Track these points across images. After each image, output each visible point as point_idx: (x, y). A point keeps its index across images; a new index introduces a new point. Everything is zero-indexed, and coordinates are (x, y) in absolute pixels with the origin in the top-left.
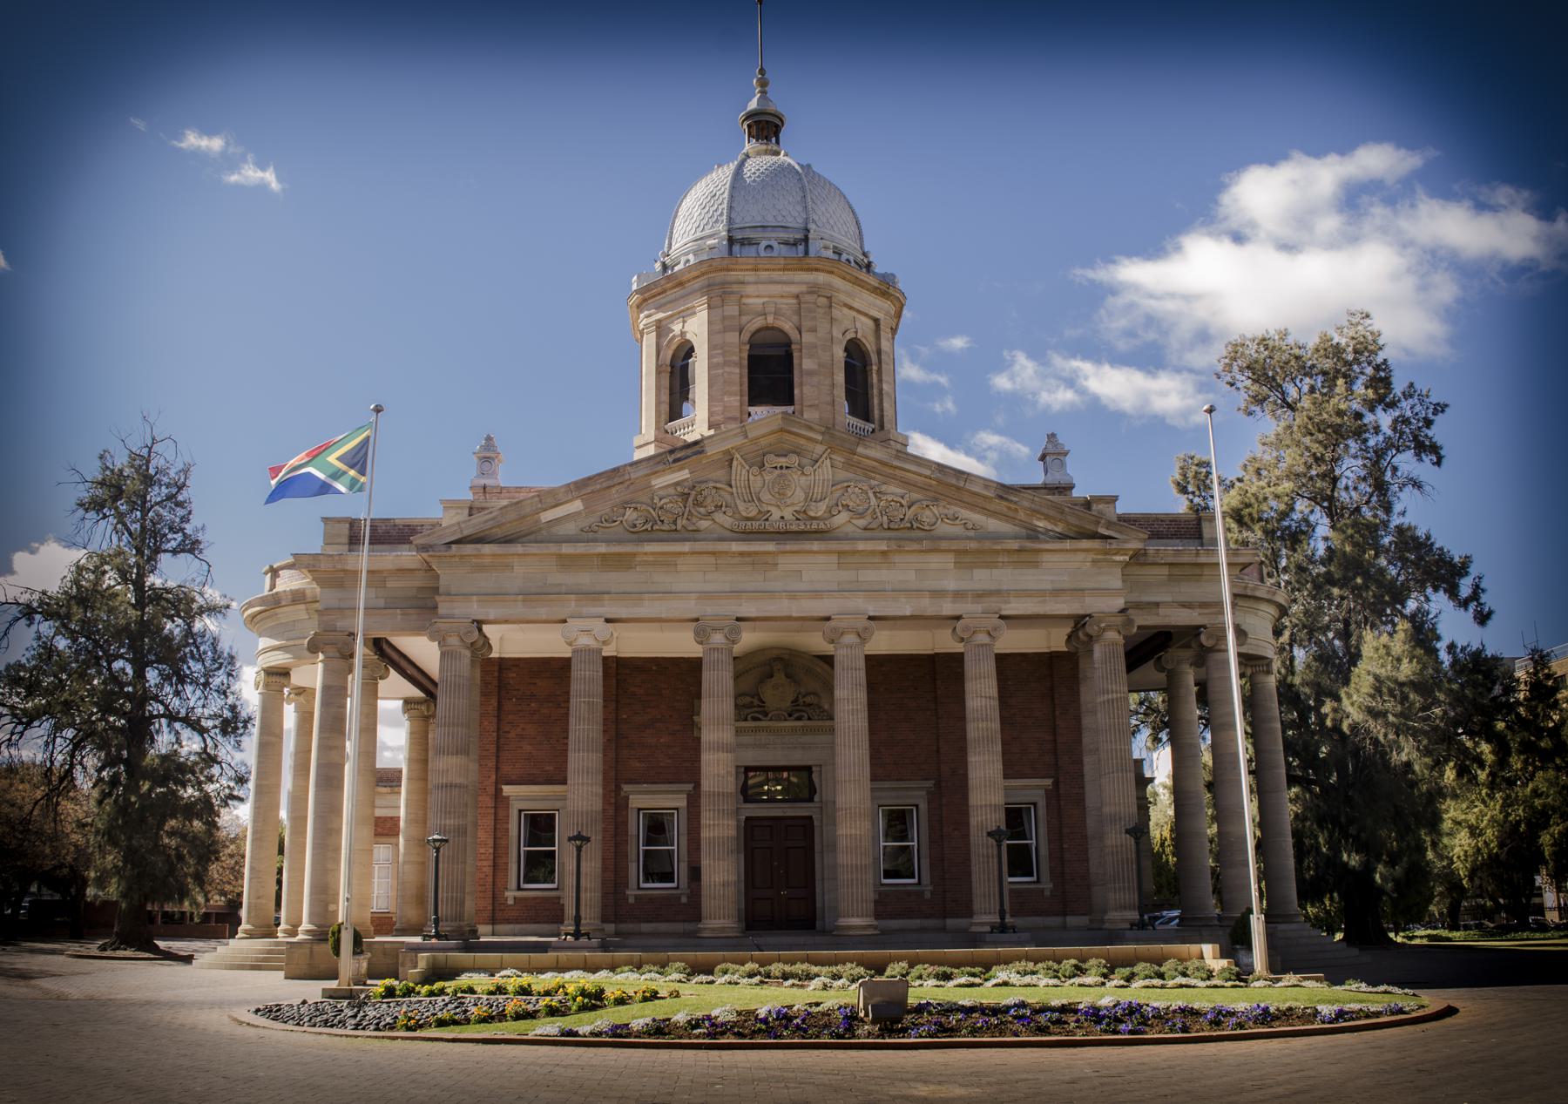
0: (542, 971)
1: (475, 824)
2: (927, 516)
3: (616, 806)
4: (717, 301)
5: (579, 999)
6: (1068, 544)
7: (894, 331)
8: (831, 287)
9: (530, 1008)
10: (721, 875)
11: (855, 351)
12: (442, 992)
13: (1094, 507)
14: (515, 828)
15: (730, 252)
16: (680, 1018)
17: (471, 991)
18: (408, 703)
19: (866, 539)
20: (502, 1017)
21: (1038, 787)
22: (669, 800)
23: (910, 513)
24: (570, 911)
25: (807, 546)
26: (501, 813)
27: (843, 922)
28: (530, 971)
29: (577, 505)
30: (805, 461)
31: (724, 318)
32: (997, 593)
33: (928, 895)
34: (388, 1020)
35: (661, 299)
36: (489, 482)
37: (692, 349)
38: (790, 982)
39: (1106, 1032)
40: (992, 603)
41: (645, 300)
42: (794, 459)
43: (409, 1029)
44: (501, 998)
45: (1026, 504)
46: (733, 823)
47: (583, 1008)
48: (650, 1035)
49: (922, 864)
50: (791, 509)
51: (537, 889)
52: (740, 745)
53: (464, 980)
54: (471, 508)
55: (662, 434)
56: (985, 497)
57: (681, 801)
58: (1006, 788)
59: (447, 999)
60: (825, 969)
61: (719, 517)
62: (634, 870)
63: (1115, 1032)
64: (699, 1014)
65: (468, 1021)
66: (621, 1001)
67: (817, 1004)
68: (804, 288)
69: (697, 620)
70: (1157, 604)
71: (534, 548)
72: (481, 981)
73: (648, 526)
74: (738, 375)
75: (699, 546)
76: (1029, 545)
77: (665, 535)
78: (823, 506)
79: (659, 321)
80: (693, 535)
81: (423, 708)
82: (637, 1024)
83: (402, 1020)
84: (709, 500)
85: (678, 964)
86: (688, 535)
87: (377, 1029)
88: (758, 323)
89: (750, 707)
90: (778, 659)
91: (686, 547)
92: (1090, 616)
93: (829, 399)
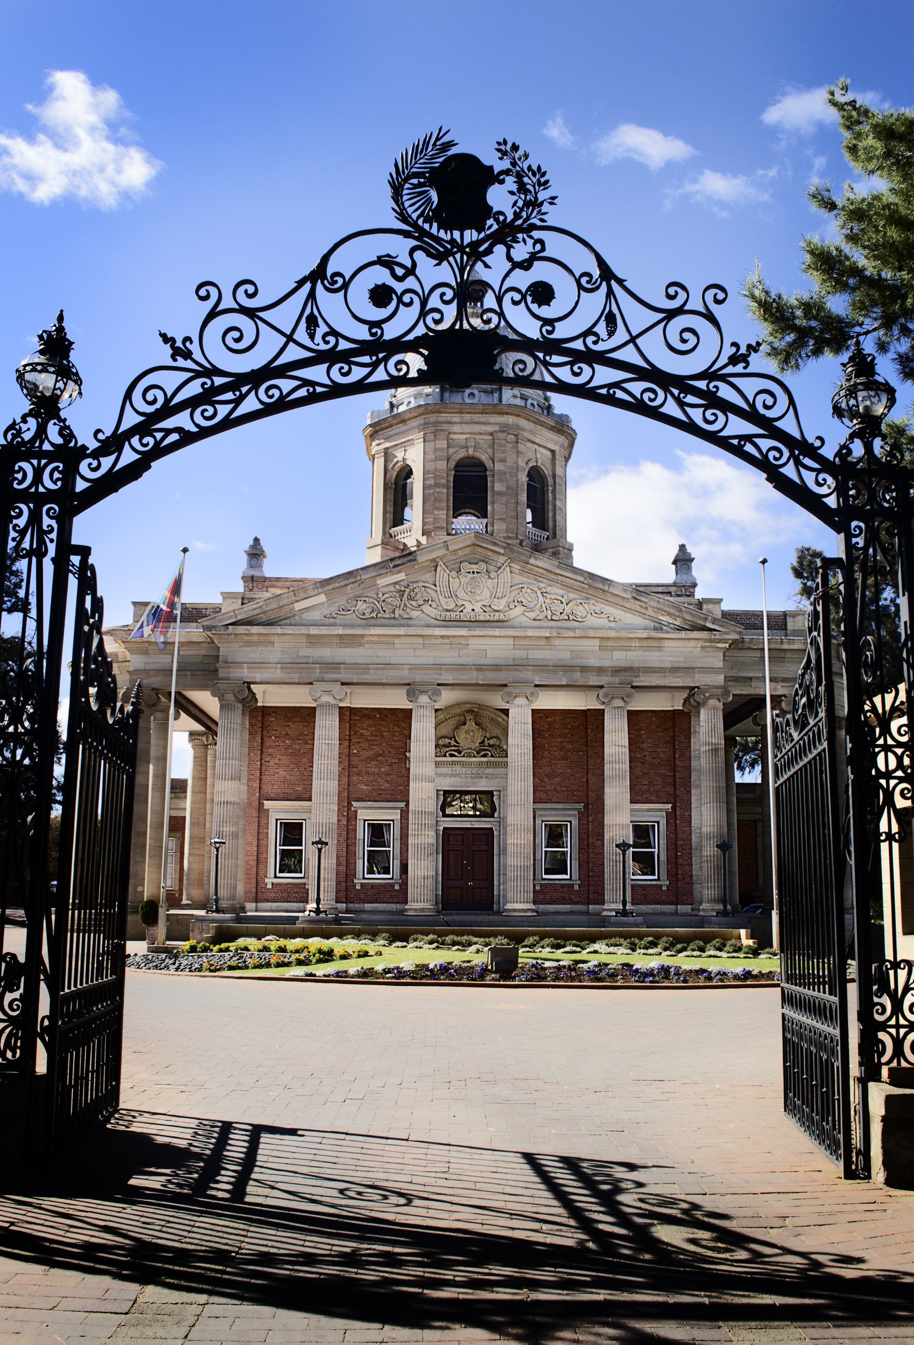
0: (294, 937)
1: (244, 830)
2: (580, 611)
3: (348, 818)
4: (431, 437)
5: (317, 955)
6: (683, 635)
7: (567, 459)
8: (518, 427)
9: (286, 960)
10: (424, 871)
11: (535, 474)
12: (227, 950)
13: (705, 607)
14: (273, 834)
15: (442, 399)
16: (379, 968)
17: (246, 949)
18: (192, 734)
19: (535, 628)
20: (268, 965)
21: (661, 810)
22: (387, 814)
23: (568, 609)
24: (313, 895)
25: (490, 632)
26: (263, 822)
27: (509, 906)
28: (285, 937)
29: (322, 598)
30: (491, 568)
31: (436, 450)
32: (631, 669)
33: (576, 888)
34: (197, 966)
35: (389, 432)
36: (256, 573)
37: (410, 473)
38: (456, 947)
39: (637, 981)
40: (626, 677)
41: (376, 432)
42: (483, 566)
43: (211, 971)
44: (267, 954)
45: (653, 604)
46: (432, 833)
47: (319, 961)
48: (359, 977)
49: (573, 865)
50: (480, 604)
51: (288, 878)
52: (439, 775)
53: (241, 942)
54: (243, 599)
55: (388, 540)
56: (623, 598)
57: (397, 815)
58: (632, 810)
59: (232, 954)
60: (482, 939)
61: (426, 608)
62: (361, 864)
63: (643, 982)
64: (392, 966)
65: (247, 967)
66: (344, 957)
67: (469, 962)
68: (497, 428)
69: (409, 684)
70: (751, 679)
71: (289, 630)
72: (252, 943)
73: (374, 615)
74: (445, 494)
75: (411, 631)
76: (655, 634)
77: (386, 622)
78: (503, 602)
79: (387, 449)
80: (407, 622)
81: (204, 739)
82: (352, 971)
83: (206, 965)
84: (419, 596)
85: (384, 935)
86: (403, 622)
87: (191, 971)
88: (462, 454)
89: (446, 746)
90: (470, 711)
91: (401, 631)
92: (698, 687)
93: (514, 514)
